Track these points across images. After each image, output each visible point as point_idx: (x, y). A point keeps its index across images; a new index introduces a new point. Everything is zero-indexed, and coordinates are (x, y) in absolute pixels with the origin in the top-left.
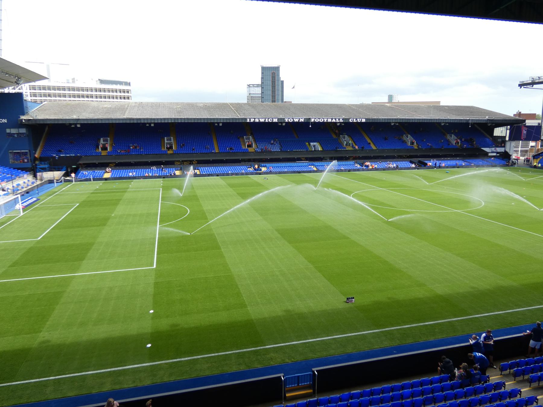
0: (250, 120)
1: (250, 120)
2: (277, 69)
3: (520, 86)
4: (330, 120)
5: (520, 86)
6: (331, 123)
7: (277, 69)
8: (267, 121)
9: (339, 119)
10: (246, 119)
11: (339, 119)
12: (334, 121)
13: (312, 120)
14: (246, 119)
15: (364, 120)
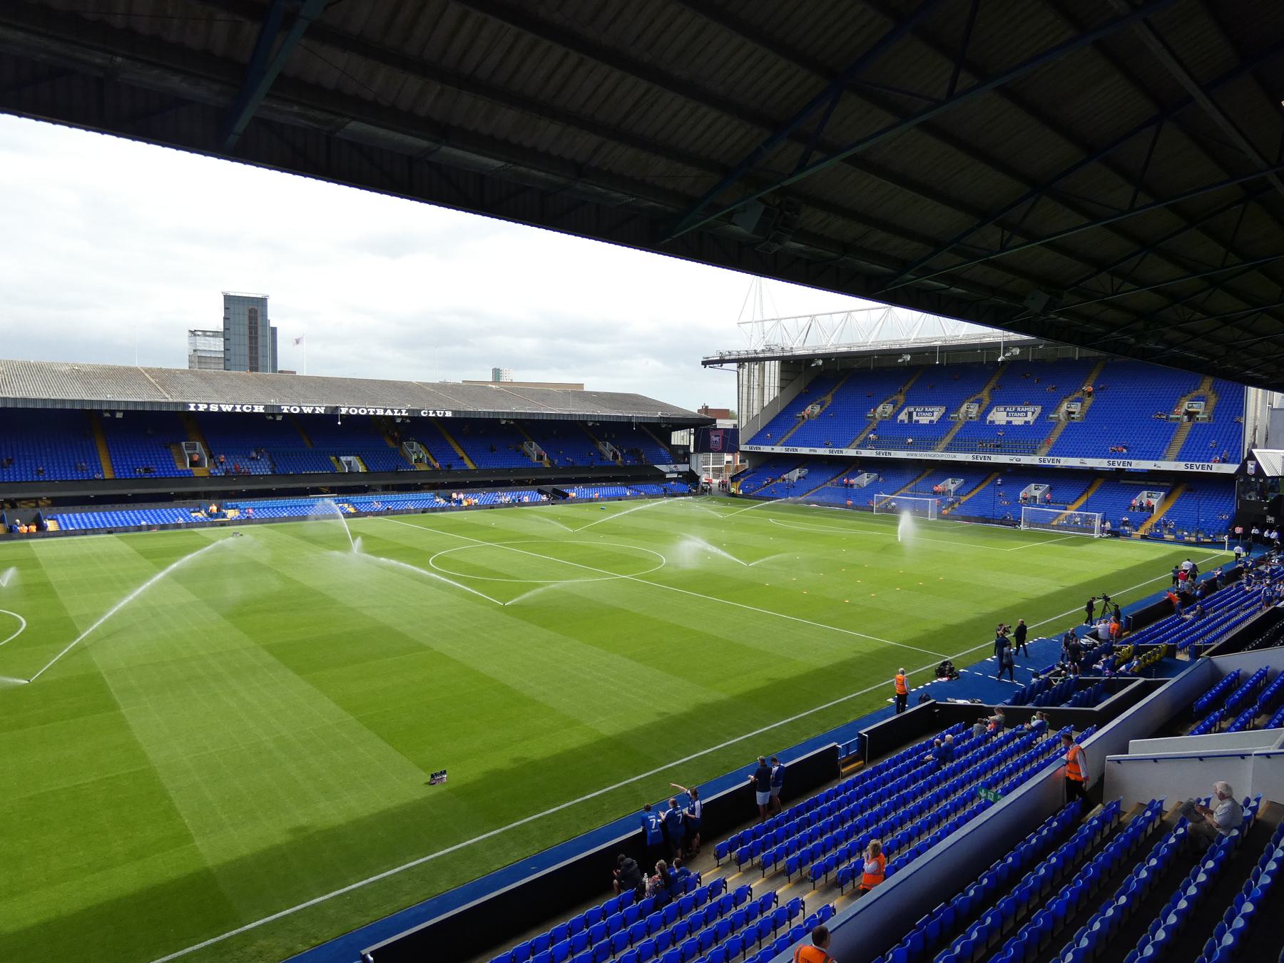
0: (197, 407)
1: (197, 407)
2: (262, 302)
3: (705, 363)
4: (381, 412)
5: (705, 363)
6: (384, 417)
7: (262, 302)
8: (238, 410)
9: (400, 411)
10: (186, 405)
11: (400, 411)
12: (389, 413)
13: (344, 411)
14: (186, 405)
15: (449, 414)
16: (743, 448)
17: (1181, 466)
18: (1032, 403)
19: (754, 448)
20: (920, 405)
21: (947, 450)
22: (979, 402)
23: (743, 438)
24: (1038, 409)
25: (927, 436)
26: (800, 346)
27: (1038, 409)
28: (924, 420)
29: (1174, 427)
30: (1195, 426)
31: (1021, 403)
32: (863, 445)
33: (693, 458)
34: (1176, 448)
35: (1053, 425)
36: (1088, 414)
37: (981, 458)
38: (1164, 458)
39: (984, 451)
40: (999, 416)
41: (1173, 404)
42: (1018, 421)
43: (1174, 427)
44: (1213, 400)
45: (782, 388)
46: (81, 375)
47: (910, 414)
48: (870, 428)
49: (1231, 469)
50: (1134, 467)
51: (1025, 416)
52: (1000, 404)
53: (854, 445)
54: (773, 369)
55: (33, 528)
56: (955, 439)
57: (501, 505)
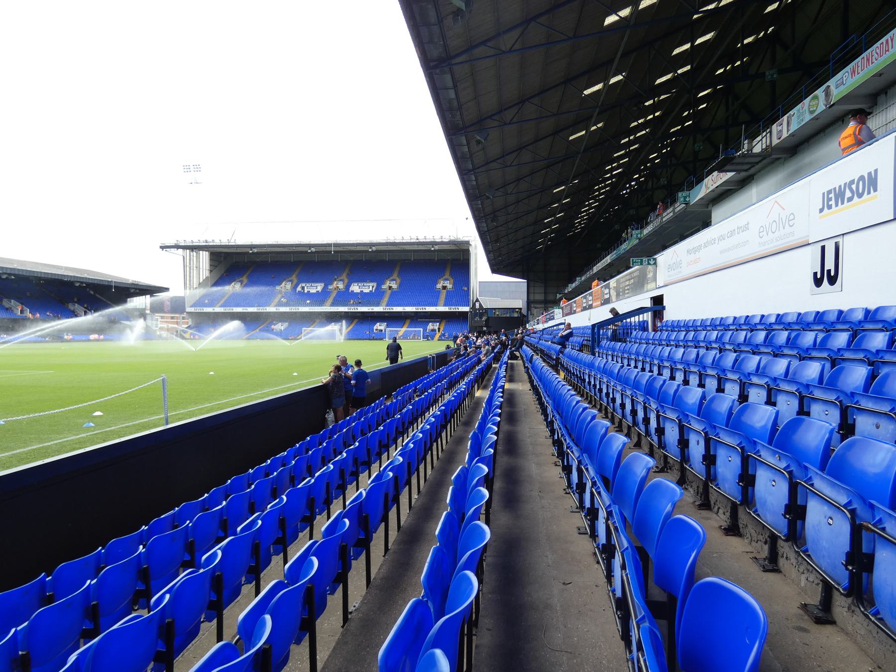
3: (162, 248)
5: (162, 248)
16: (188, 310)
18: (371, 281)
19: (199, 310)
20: (308, 282)
22: (291, 281)
28: (313, 291)
29: (439, 292)
30: (448, 291)
31: (366, 282)
33: (148, 317)
34: (330, 300)
36: (400, 286)
37: (420, 309)
38: (269, 305)
40: (355, 288)
41: (436, 283)
42: (366, 290)
43: (439, 292)
44: (398, 281)
45: (211, 271)
46: (67, 268)
47: (303, 288)
49: (466, 309)
51: (368, 288)
54: (205, 256)
55: (524, 347)
56: (334, 299)
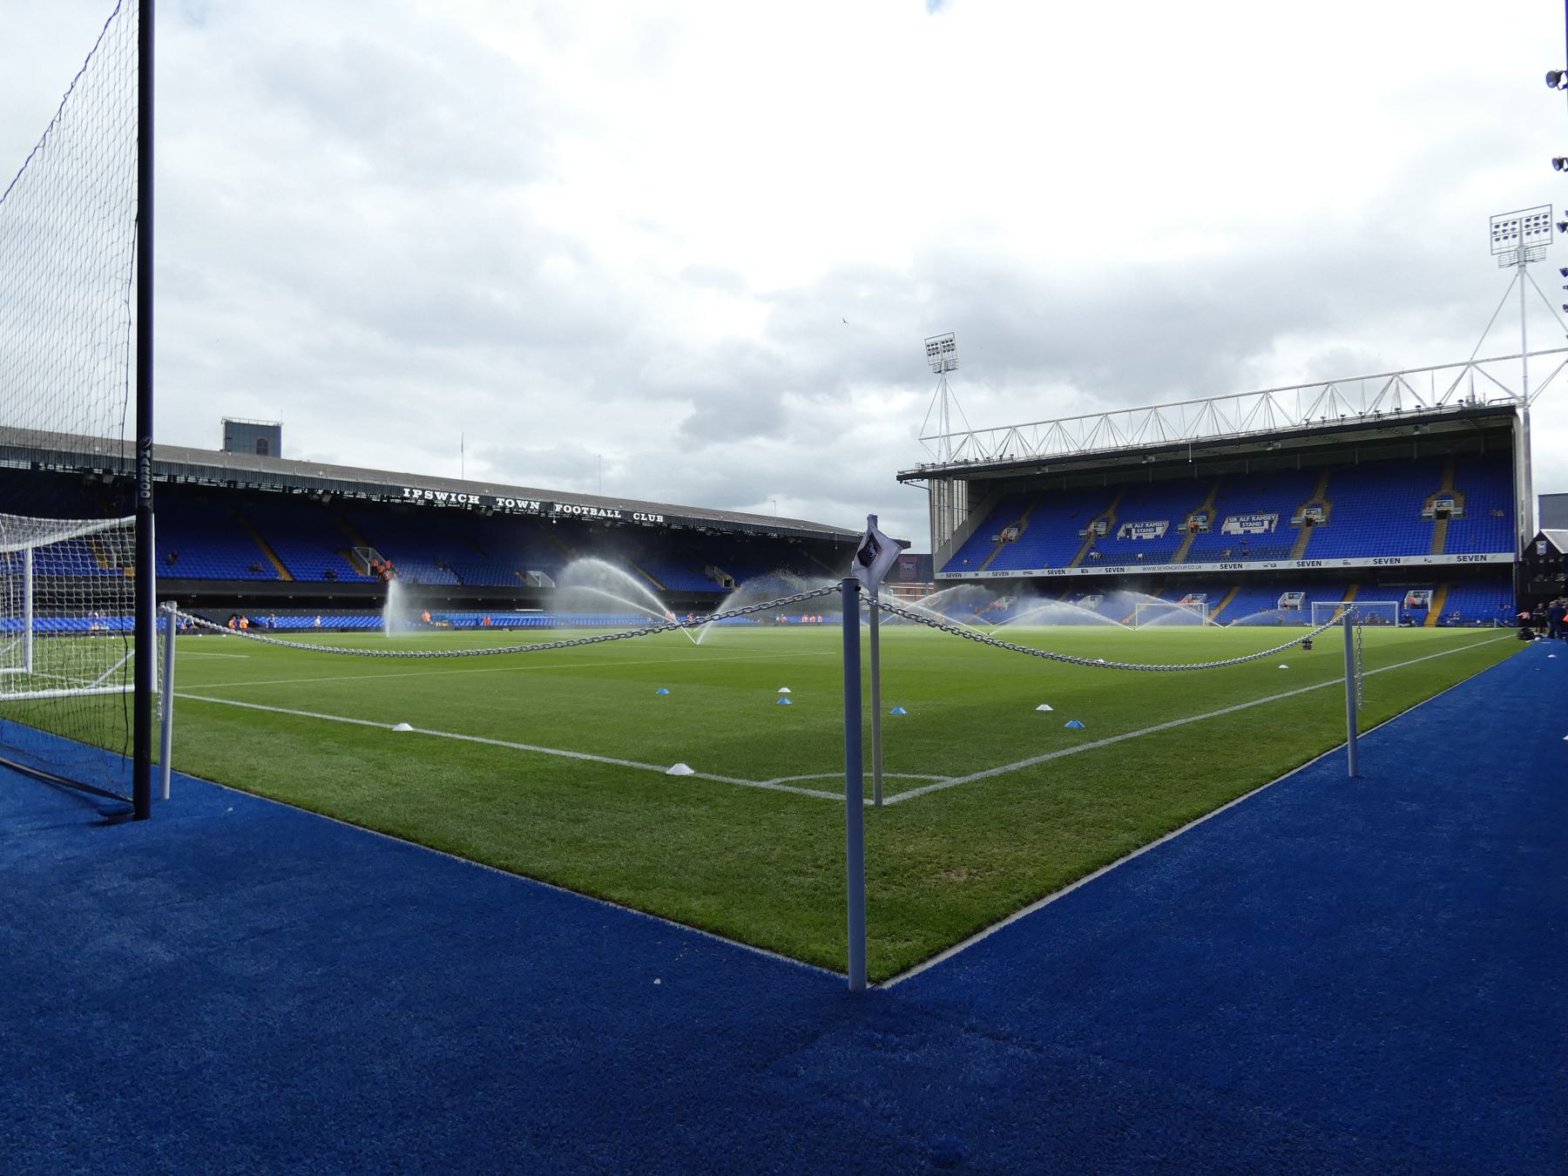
1: (411, 493)
3: (902, 478)
16: (939, 576)
17: (1453, 559)
20: (1139, 520)
21: (1188, 559)
22: (1107, 521)
23: (937, 565)
24: (1166, 524)
25: (1159, 550)
26: (985, 449)
27: (1166, 524)
28: (1148, 535)
30: (1314, 534)
32: (1088, 562)
34: (1184, 551)
35: (1296, 531)
39: (1233, 557)
40: (1233, 526)
41: (1421, 506)
44: (1328, 508)
47: (1128, 531)
48: (1086, 547)
49: (1507, 558)
50: (1489, 561)
51: (1260, 525)
52: (1233, 515)
53: (1077, 561)
54: (960, 487)
57: (313, 629)
